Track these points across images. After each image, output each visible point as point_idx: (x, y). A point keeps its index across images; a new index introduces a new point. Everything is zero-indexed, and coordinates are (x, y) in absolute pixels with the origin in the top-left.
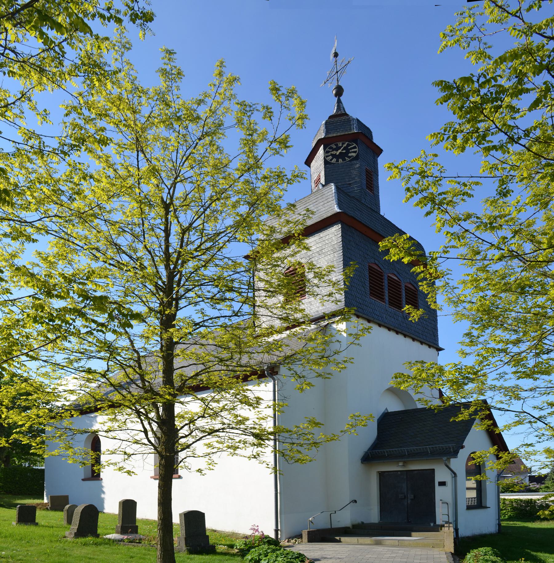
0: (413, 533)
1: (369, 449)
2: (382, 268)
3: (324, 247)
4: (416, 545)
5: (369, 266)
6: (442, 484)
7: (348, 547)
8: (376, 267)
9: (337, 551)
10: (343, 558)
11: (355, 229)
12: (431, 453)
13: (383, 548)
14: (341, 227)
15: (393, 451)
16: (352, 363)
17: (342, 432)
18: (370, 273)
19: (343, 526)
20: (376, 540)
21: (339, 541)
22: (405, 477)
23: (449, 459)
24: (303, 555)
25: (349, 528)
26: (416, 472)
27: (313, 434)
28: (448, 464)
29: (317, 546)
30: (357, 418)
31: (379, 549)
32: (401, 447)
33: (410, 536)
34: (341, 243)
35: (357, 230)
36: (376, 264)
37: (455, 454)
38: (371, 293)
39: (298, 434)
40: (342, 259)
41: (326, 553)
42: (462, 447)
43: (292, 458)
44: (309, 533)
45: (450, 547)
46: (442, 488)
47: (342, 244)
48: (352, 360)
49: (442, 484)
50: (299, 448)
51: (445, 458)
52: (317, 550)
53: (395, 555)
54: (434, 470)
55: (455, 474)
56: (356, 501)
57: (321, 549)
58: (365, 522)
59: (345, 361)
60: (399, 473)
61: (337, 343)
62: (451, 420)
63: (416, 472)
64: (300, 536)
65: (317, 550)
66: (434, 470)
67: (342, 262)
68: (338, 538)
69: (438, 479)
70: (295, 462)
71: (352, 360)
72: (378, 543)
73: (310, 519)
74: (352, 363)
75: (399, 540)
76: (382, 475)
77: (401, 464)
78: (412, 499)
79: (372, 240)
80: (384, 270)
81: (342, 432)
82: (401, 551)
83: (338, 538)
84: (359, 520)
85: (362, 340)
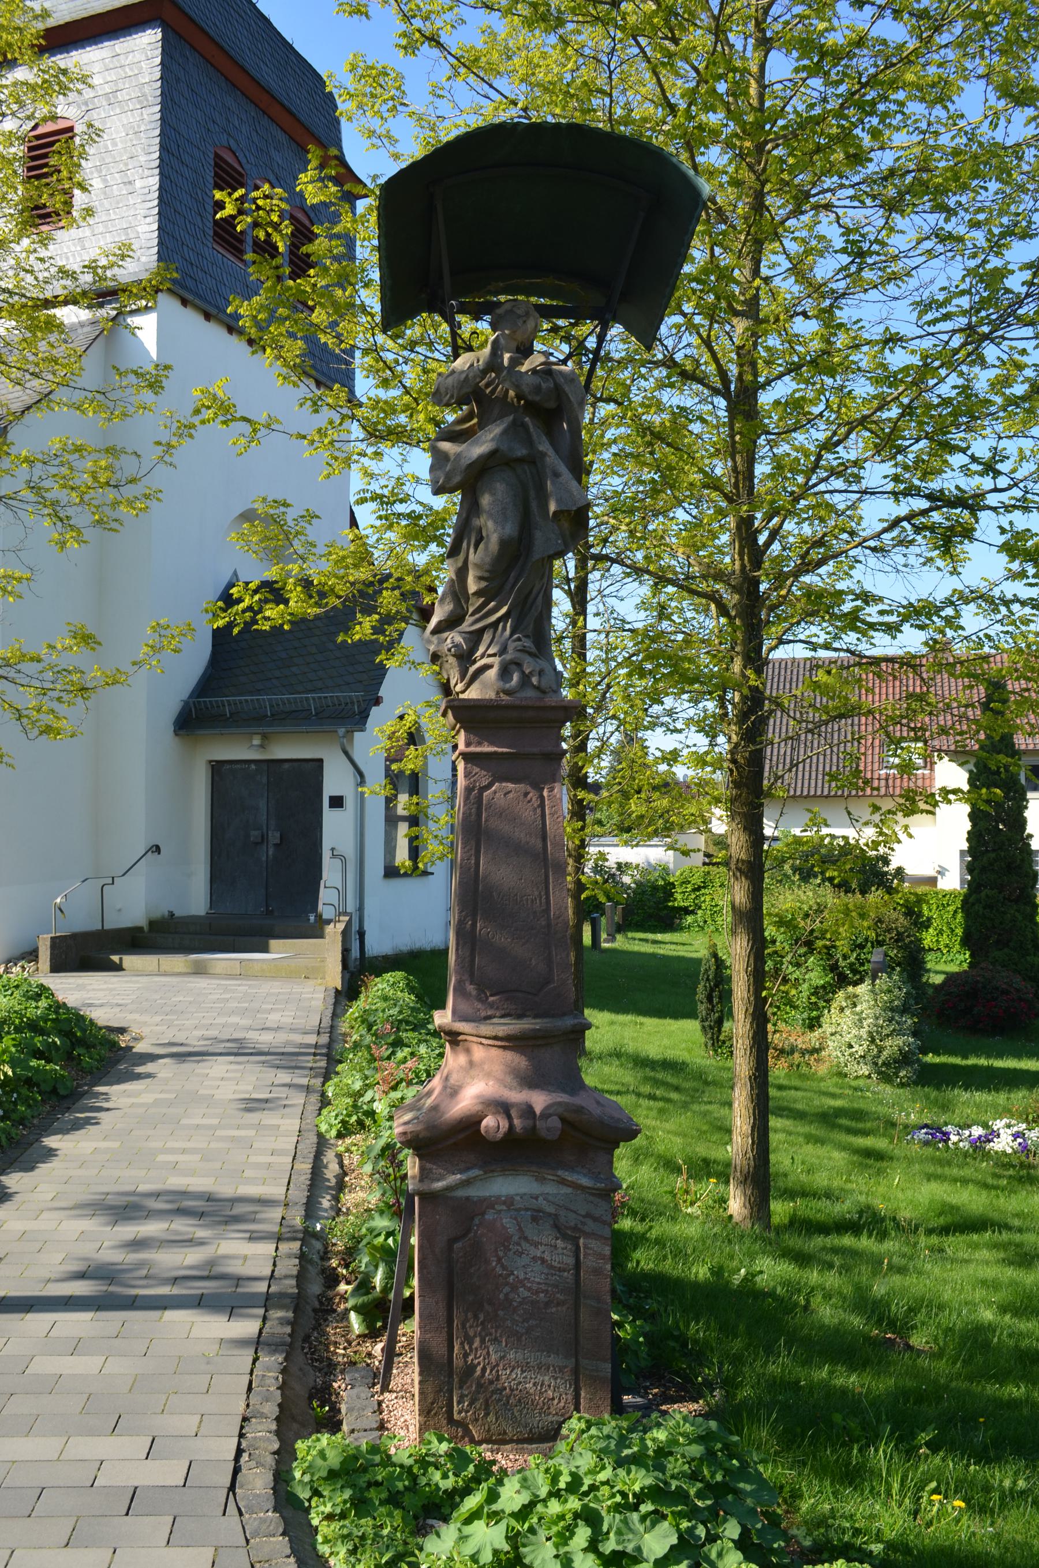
0: (273, 943)
1: (190, 697)
2: (243, 161)
3: (121, 87)
4: (274, 973)
5: (217, 155)
6: (337, 802)
7: (137, 982)
8: (230, 159)
9: (114, 989)
10: (126, 1005)
11: (191, 46)
12: (317, 714)
13: (208, 981)
14: (163, 39)
15: (241, 702)
16: (158, 500)
17: (134, 663)
18: (216, 174)
19: (130, 925)
20: (197, 963)
21: (118, 968)
22: (264, 780)
23: (350, 733)
24: (49, 989)
25: (139, 929)
26: (286, 766)
27: (83, 672)
28: (348, 749)
29: (71, 980)
30: (163, 632)
31: (201, 983)
32: (258, 692)
33: (265, 950)
34: (159, 83)
35: (195, 49)
36: (230, 149)
37: (360, 719)
38: (216, 233)
39: (56, 670)
40: (158, 132)
41: (91, 994)
42: (378, 701)
43: (34, 723)
44: (56, 943)
45: (334, 978)
46: (337, 813)
47: (162, 87)
48: (159, 495)
49: (337, 802)
50: (55, 705)
51: (341, 731)
52: (70, 989)
53: (228, 996)
54: (321, 761)
55: (361, 774)
56: (157, 849)
57: (80, 988)
58: (178, 913)
59: (147, 497)
60: (253, 767)
61: (134, 457)
62: (340, 639)
63: (286, 766)
64: (32, 955)
65: (70, 989)
66: (321, 761)
67: (158, 140)
68: (115, 958)
69: (331, 787)
70: (41, 733)
71: (159, 495)
72: (200, 971)
73: (58, 900)
74: (158, 500)
75: (241, 961)
76: (217, 768)
77: (256, 741)
78: (276, 845)
79: (227, 79)
80: (247, 166)
81: (134, 663)
82: (242, 987)
83: (115, 958)
84: (161, 911)
85: (177, 457)
